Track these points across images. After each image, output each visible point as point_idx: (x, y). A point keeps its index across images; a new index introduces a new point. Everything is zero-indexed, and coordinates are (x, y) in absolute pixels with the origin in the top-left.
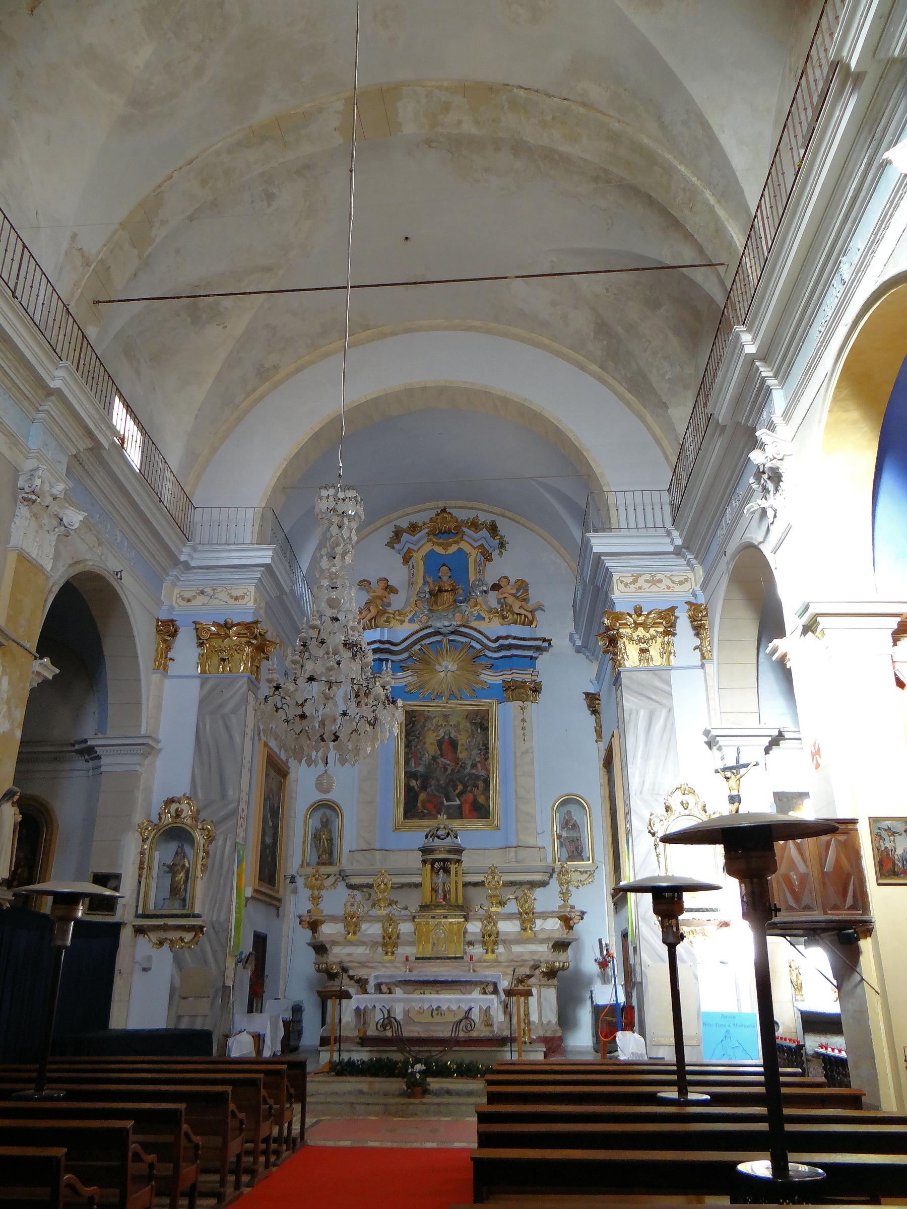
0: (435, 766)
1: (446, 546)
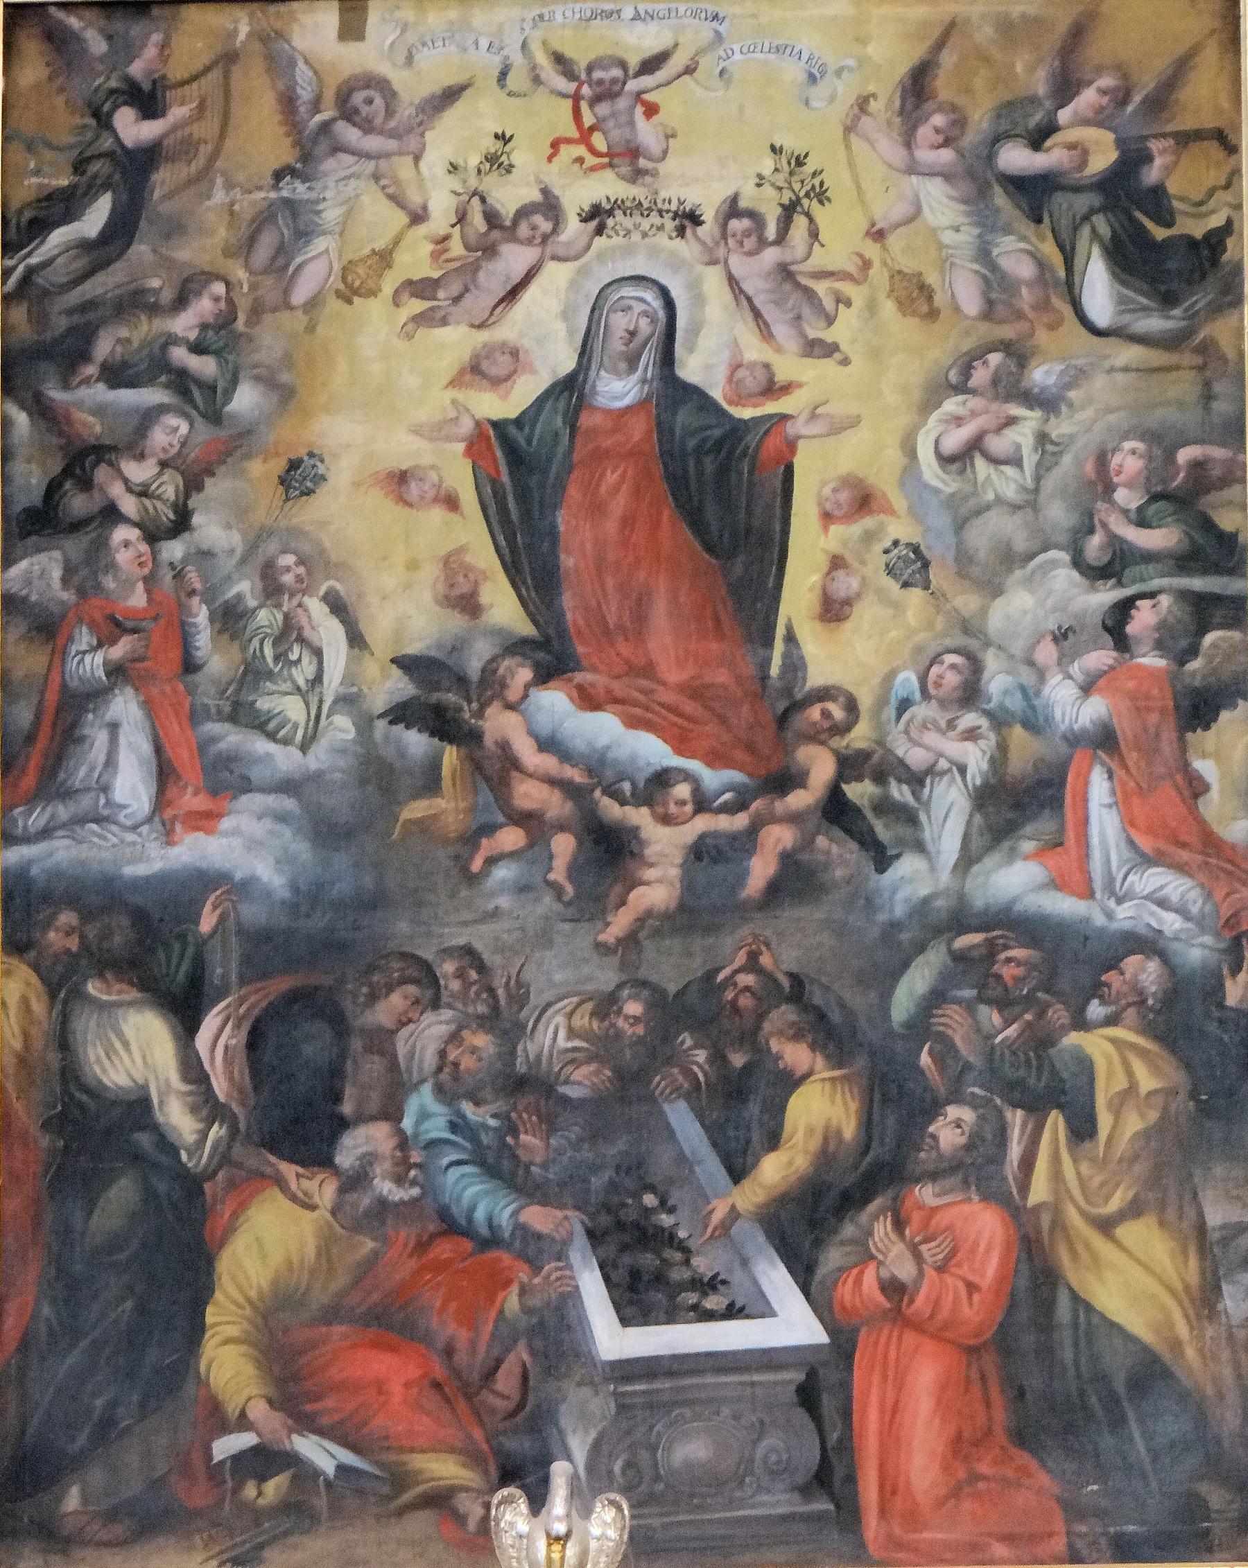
0: (448, 808)
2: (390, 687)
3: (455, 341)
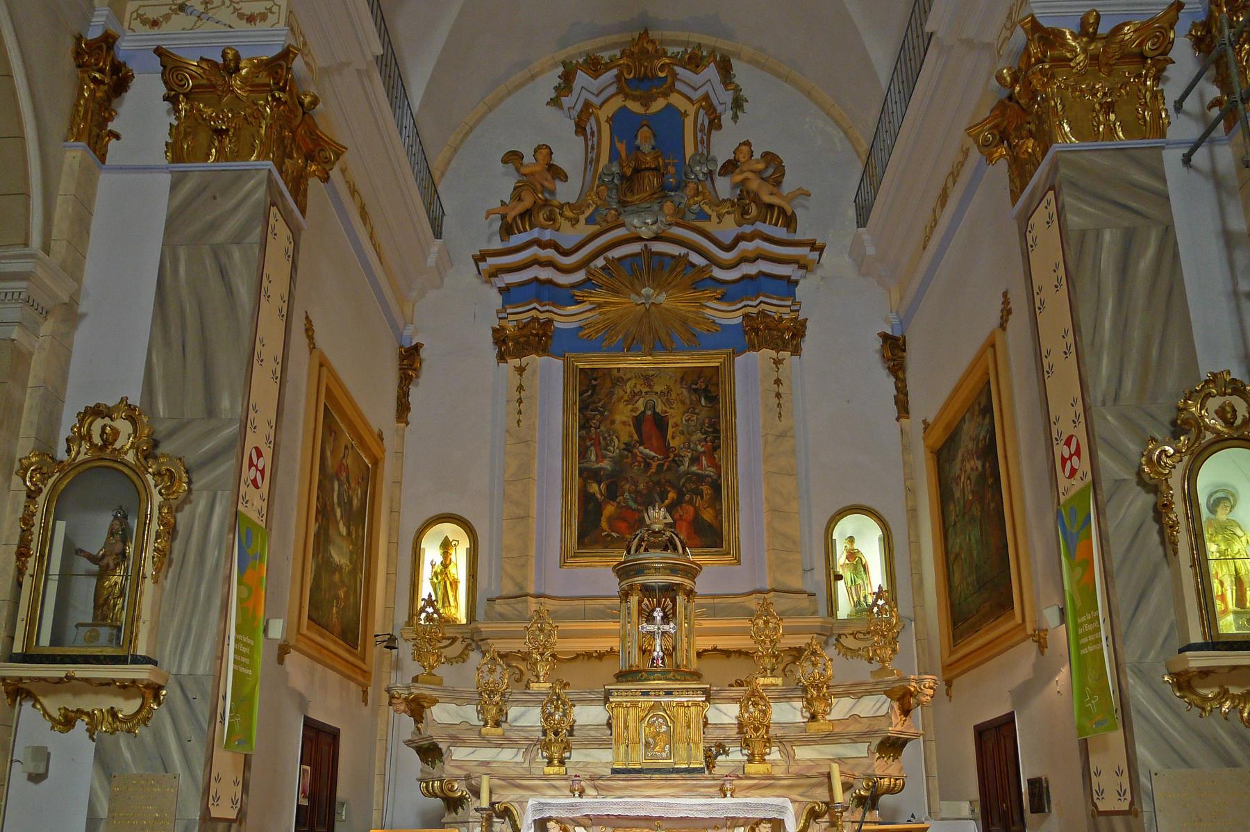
0: (629, 460)
1: (646, 101)
2: (623, 446)
3: (630, 407)
